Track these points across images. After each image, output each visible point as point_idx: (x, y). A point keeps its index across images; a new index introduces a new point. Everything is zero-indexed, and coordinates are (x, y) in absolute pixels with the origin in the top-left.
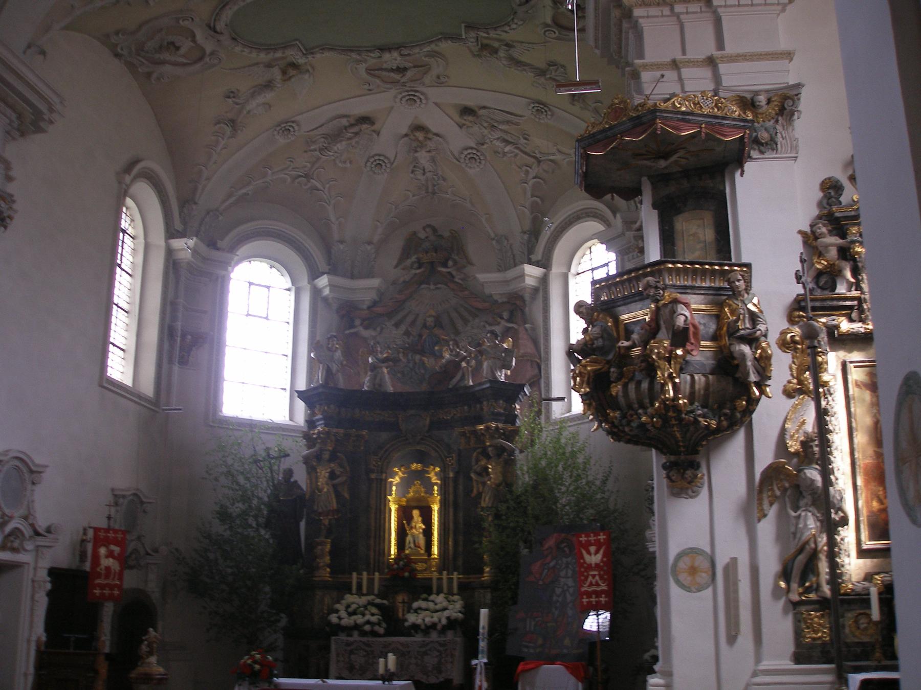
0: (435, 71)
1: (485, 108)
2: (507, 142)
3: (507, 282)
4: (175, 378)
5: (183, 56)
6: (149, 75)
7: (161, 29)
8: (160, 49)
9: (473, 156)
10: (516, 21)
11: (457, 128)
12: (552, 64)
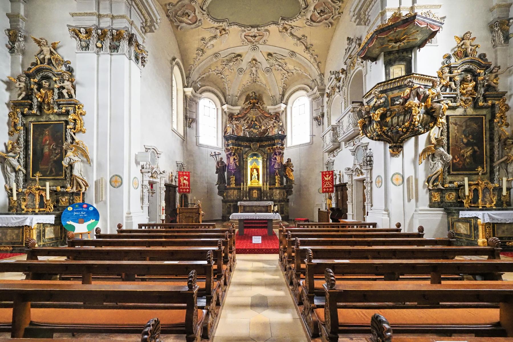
2: (280, 66)
4: (188, 131)
6: (178, 26)
9: (268, 70)
12: (304, 36)
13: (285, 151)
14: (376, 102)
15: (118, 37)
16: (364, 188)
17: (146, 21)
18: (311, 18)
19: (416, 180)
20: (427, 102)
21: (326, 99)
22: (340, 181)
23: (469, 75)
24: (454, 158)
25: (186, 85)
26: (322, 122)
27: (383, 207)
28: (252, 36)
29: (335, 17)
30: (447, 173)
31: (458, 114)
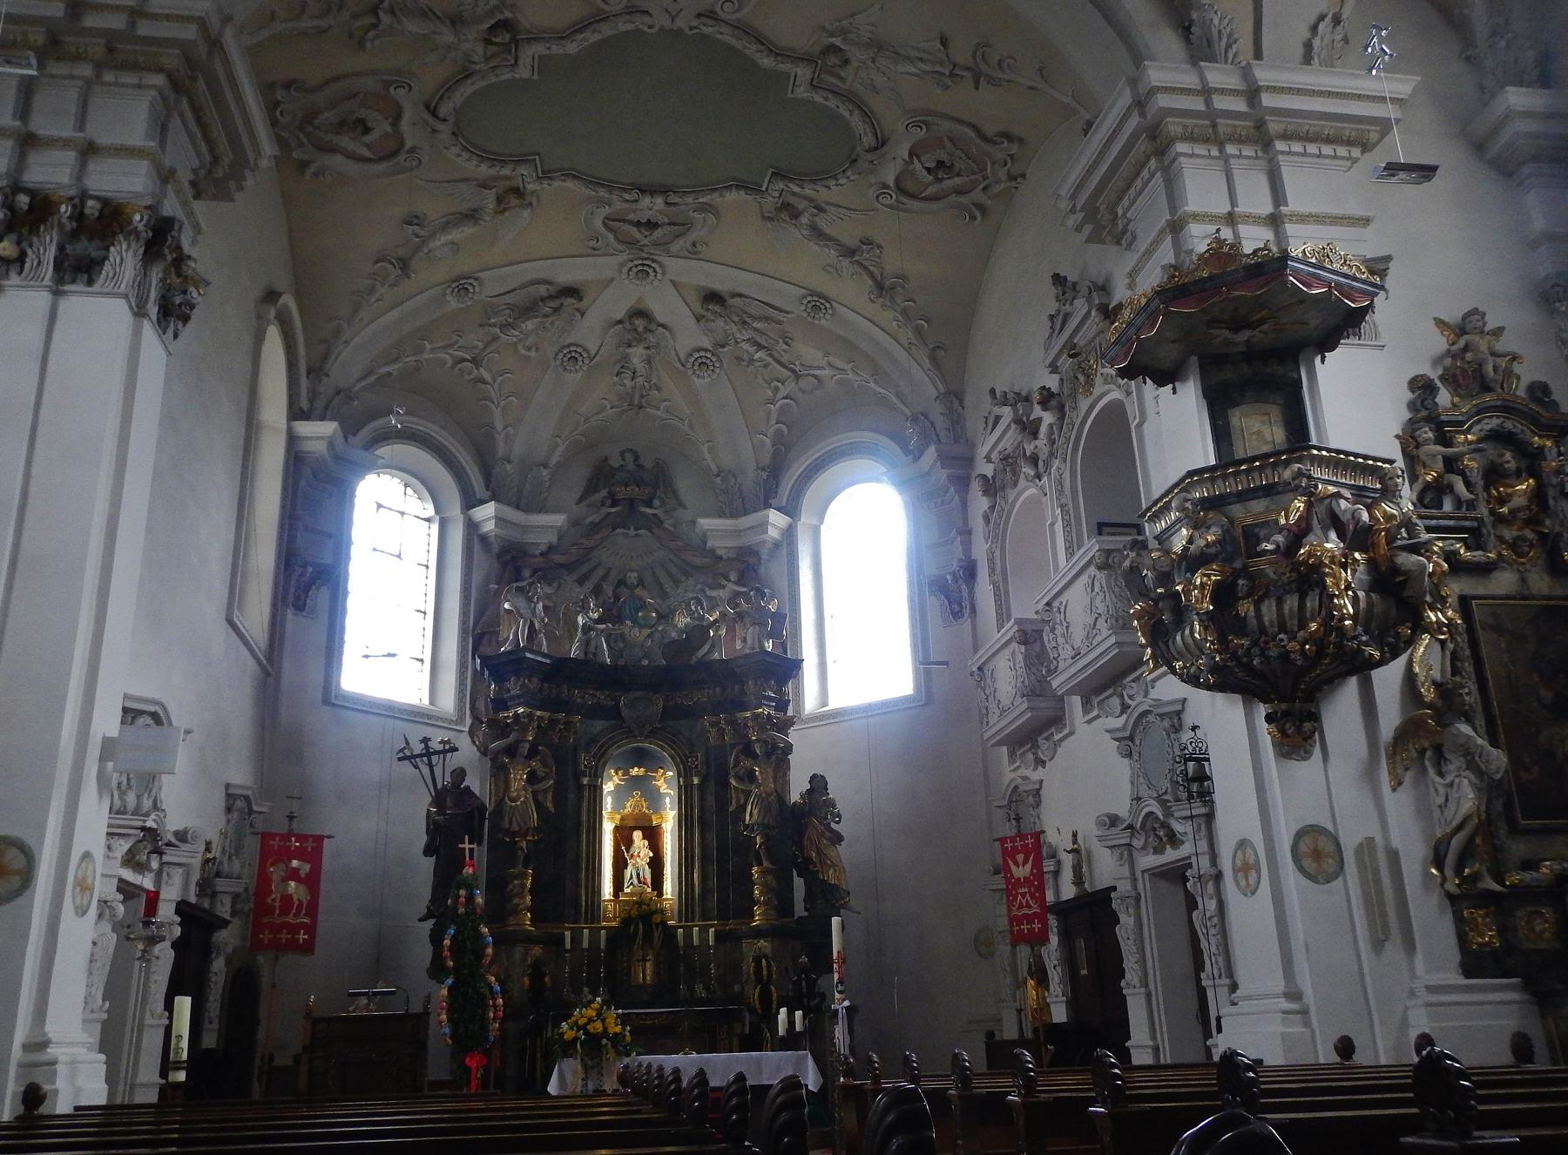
0: (693, 236)
1: (740, 295)
2: (760, 346)
3: (738, 533)
4: (289, 626)
5: (367, 146)
6: (304, 165)
7: (356, 95)
8: (341, 126)
9: (703, 361)
10: (849, 173)
11: (693, 321)
12: (867, 241)
13: (793, 736)
14: (1190, 541)
15: (107, 222)
16: (1191, 904)
17: (216, 160)
18: (897, 181)
19: (1394, 856)
20: (1375, 546)
21: (980, 503)
22: (1078, 880)
23: (1508, 456)
24: (1515, 761)
25: (304, 404)
26: (966, 603)
27: (1279, 985)
28: (638, 224)
29: (996, 189)
30: (1503, 831)
31: (1501, 591)
